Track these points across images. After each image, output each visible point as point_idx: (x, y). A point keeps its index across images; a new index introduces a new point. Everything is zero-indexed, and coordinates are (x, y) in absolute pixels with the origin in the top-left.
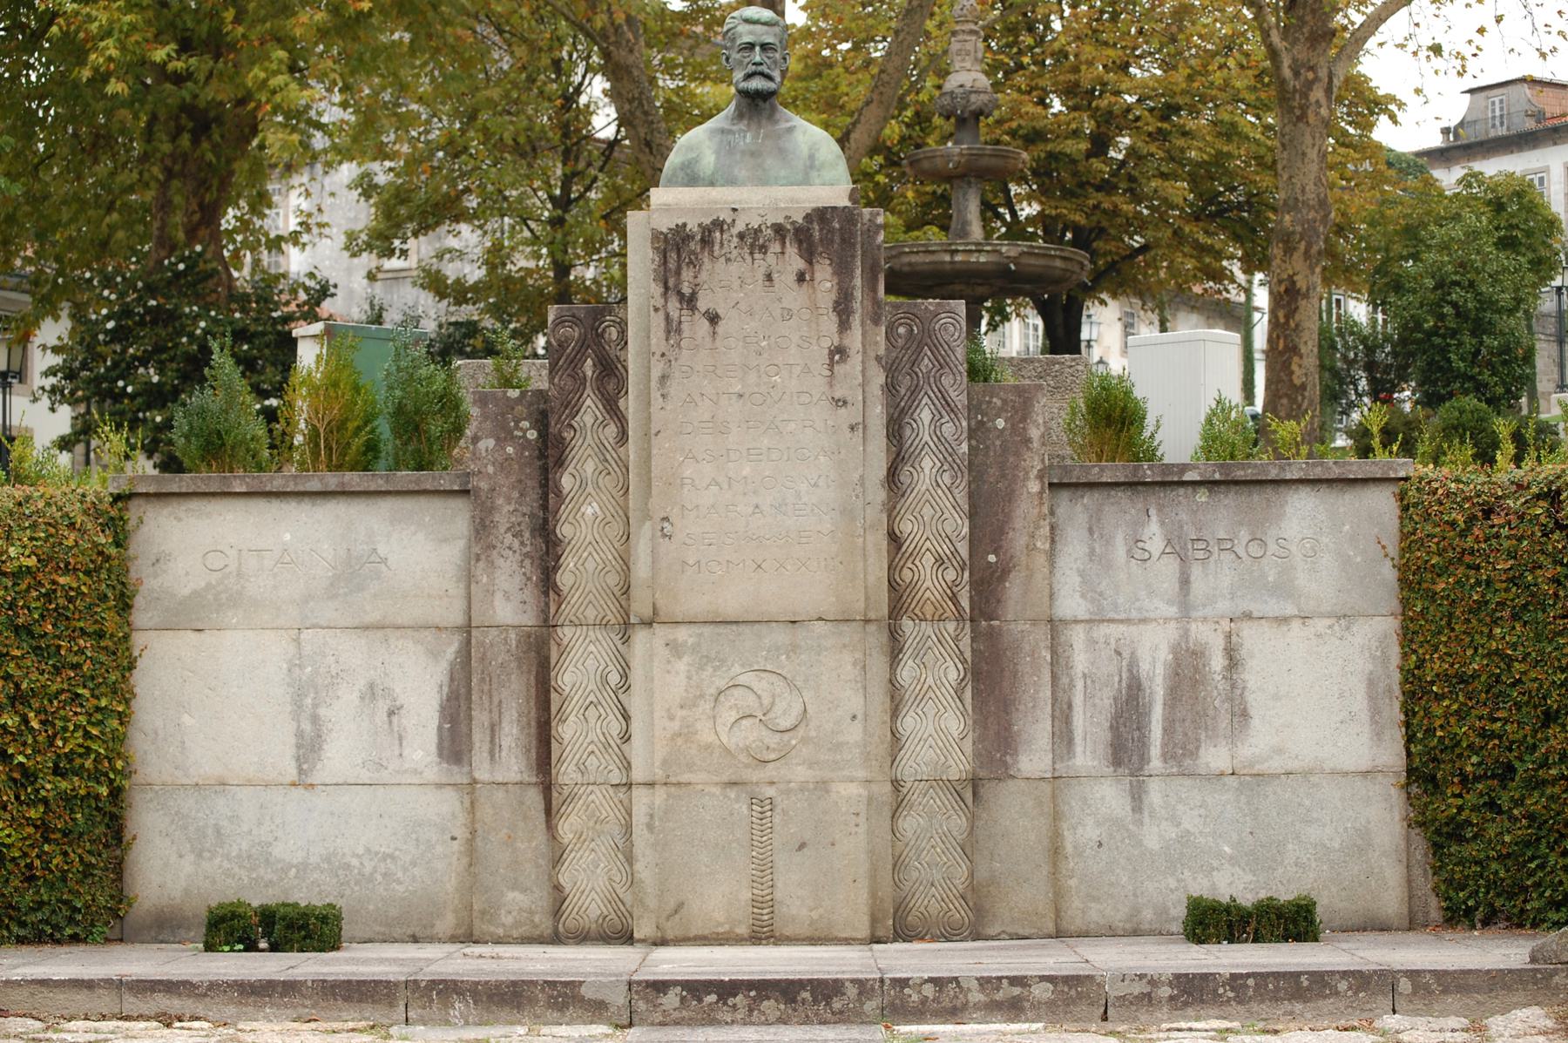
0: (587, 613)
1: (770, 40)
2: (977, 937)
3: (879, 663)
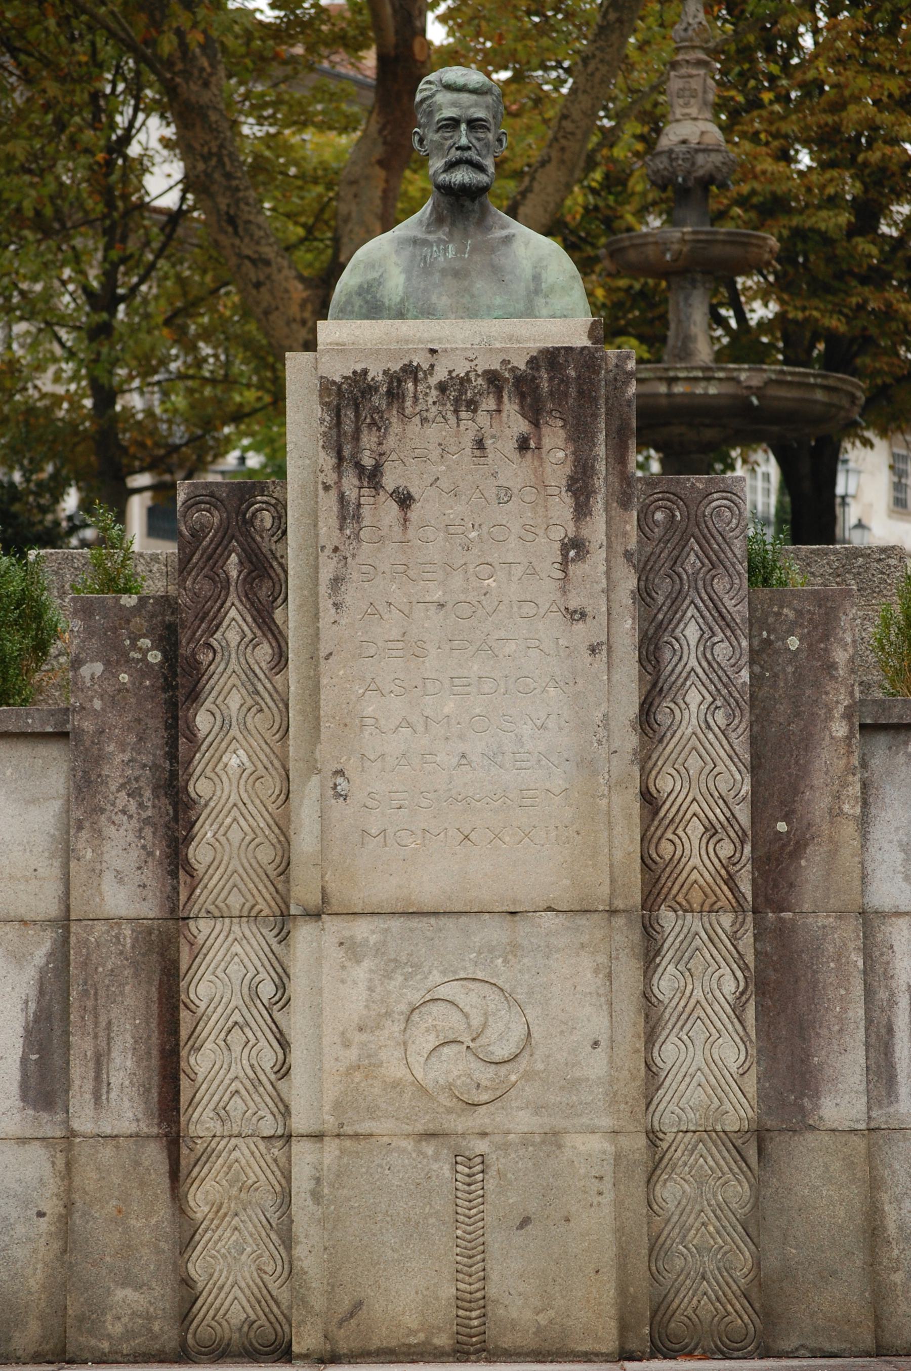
0: (231, 900)
1: (480, 114)
2: (766, 1353)
3: (629, 971)
